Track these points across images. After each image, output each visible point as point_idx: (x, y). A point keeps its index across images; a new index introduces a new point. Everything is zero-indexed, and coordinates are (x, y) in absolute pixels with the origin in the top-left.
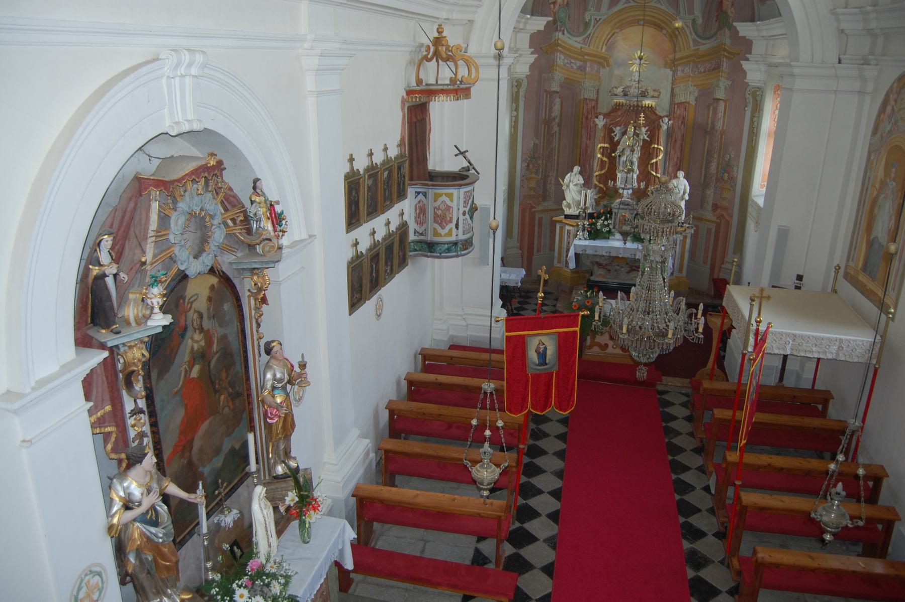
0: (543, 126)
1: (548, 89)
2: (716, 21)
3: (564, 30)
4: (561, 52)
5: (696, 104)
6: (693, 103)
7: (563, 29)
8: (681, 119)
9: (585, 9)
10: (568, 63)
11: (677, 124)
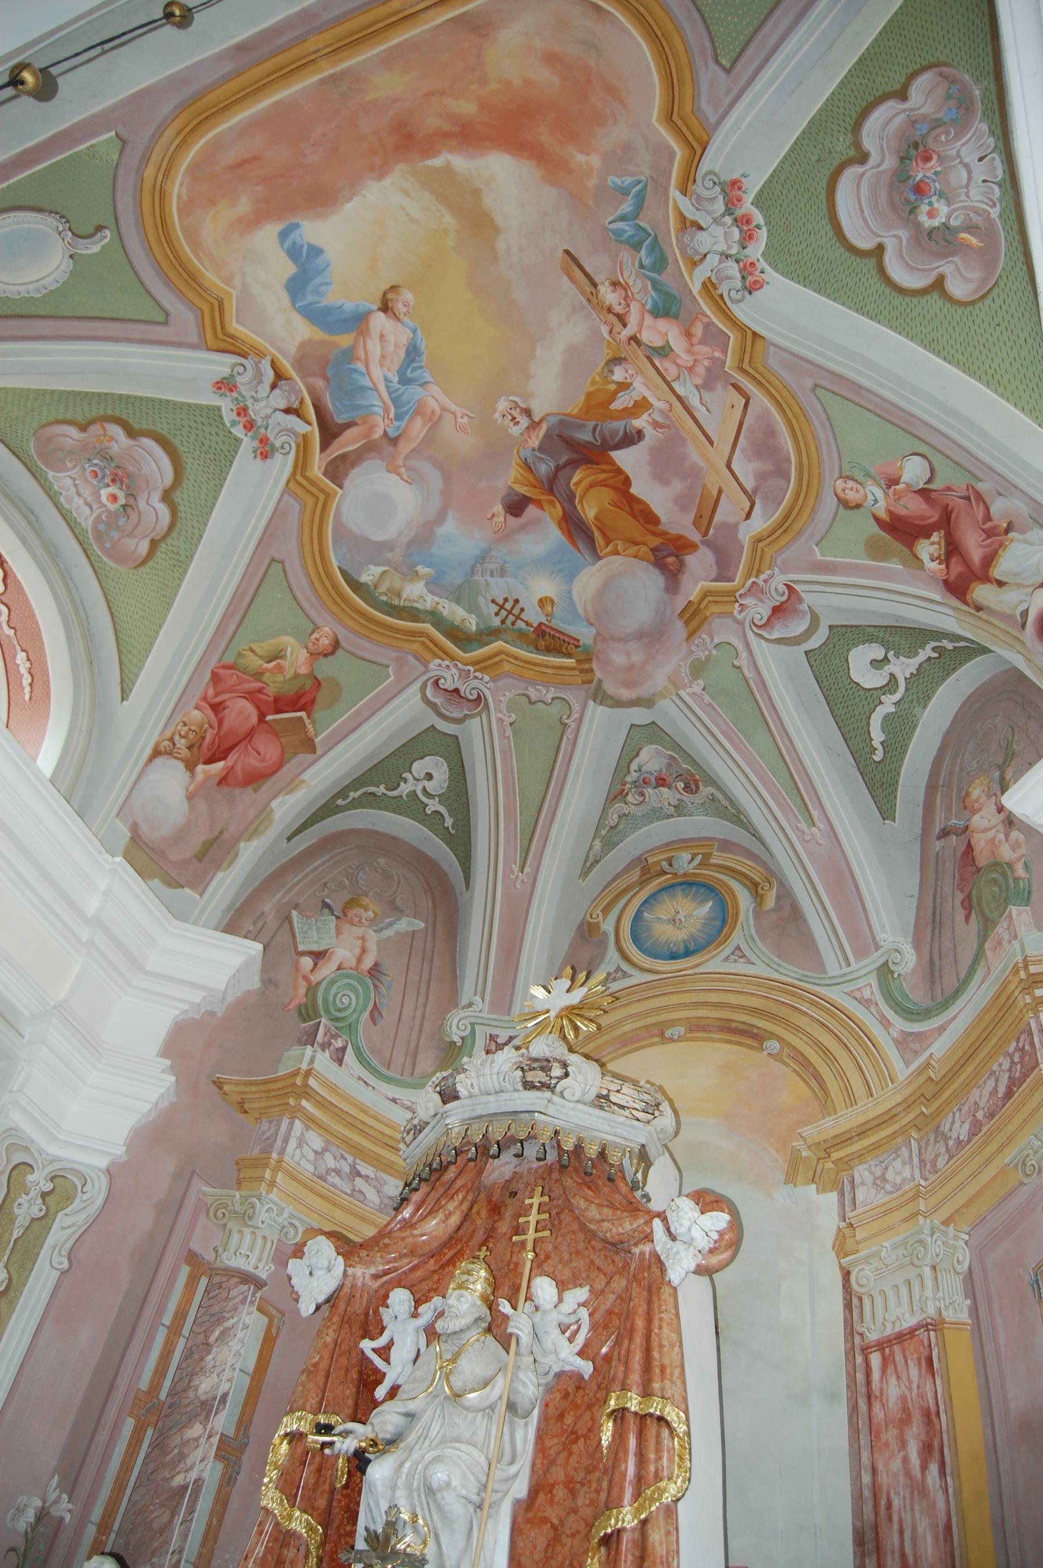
0: (130, 1423)
1: (209, 1256)
2: (967, 918)
3: (343, 1049)
4: (312, 1122)
5: (974, 1310)
6: (959, 1312)
7: (339, 1043)
8: (915, 1431)
9: (452, 999)
10: (338, 1172)
11: (896, 1464)
